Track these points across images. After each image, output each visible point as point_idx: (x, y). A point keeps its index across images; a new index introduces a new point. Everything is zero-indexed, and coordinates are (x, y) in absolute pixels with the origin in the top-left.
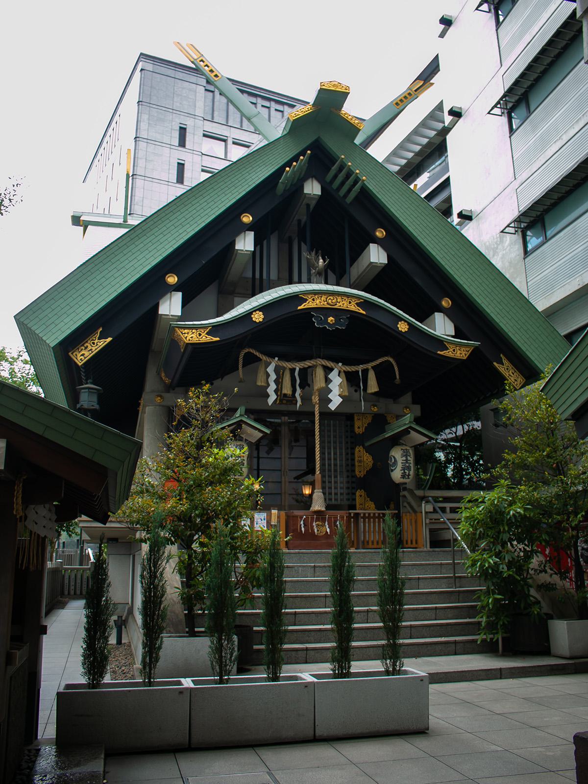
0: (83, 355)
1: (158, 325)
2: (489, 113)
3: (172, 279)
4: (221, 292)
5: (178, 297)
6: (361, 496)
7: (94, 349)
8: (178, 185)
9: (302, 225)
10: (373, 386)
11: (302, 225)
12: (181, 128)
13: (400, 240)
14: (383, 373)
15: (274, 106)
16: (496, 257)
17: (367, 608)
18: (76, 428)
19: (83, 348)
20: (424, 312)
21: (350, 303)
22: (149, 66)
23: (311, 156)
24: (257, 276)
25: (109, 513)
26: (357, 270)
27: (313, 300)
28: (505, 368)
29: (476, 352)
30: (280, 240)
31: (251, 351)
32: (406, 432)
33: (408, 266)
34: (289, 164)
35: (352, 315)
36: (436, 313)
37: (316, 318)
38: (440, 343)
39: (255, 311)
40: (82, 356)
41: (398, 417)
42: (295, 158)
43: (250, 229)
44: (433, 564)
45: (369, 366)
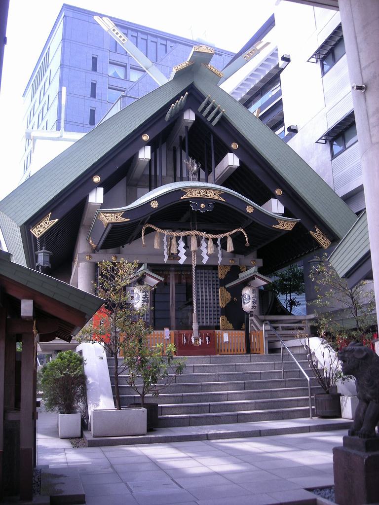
0: (39, 231)
1: (87, 210)
2: (308, 61)
3: (97, 179)
4: (128, 185)
5: (101, 191)
6: (223, 320)
7: (46, 227)
8: (92, 99)
9: (183, 139)
10: (230, 247)
11: (183, 139)
12: (93, 58)
13: (247, 150)
14: (237, 239)
15: (160, 41)
16: (313, 159)
17: (227, 392)
18: (44, 282)
19: (39, 226)
20: (263, 197)
21: (215, 194)
22: (70, 14)
23: (188, 96)
24: (153, 173)
25: (72, 336)
26: (220, 169)
27: (191, 192)
28: (318, 236)
29: (298, 225)
30: (168, 149)
31: (150, 226)
32: (253, 278)
33: (254, 168)
34: (173, 101)
35: (217, 204)
36: (272, 199)
37: (193, 204)
38: (273, 220)
39: (153, 201)
40: (38, 231)
41: (248, 268)
42: (178, 97)
43: (148, 145)
44: (270, 364)
45: (227, 234)
